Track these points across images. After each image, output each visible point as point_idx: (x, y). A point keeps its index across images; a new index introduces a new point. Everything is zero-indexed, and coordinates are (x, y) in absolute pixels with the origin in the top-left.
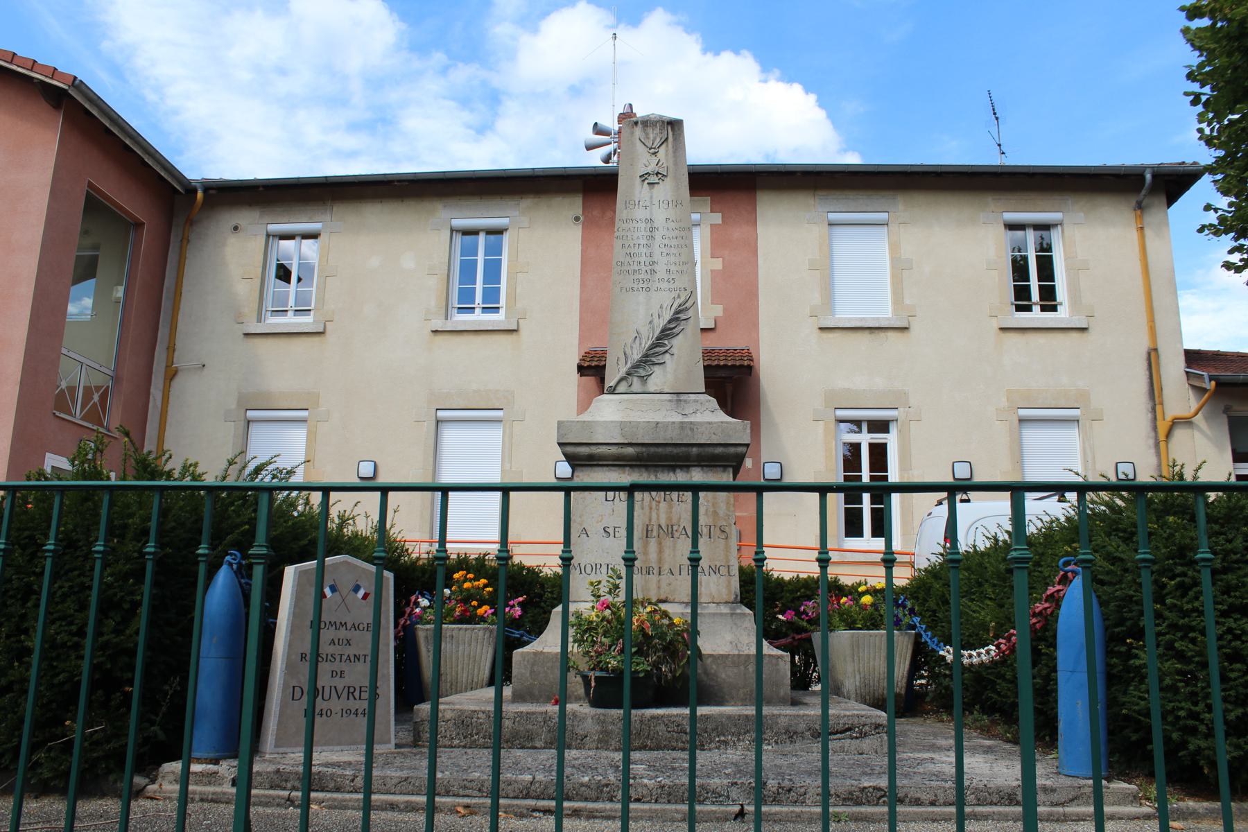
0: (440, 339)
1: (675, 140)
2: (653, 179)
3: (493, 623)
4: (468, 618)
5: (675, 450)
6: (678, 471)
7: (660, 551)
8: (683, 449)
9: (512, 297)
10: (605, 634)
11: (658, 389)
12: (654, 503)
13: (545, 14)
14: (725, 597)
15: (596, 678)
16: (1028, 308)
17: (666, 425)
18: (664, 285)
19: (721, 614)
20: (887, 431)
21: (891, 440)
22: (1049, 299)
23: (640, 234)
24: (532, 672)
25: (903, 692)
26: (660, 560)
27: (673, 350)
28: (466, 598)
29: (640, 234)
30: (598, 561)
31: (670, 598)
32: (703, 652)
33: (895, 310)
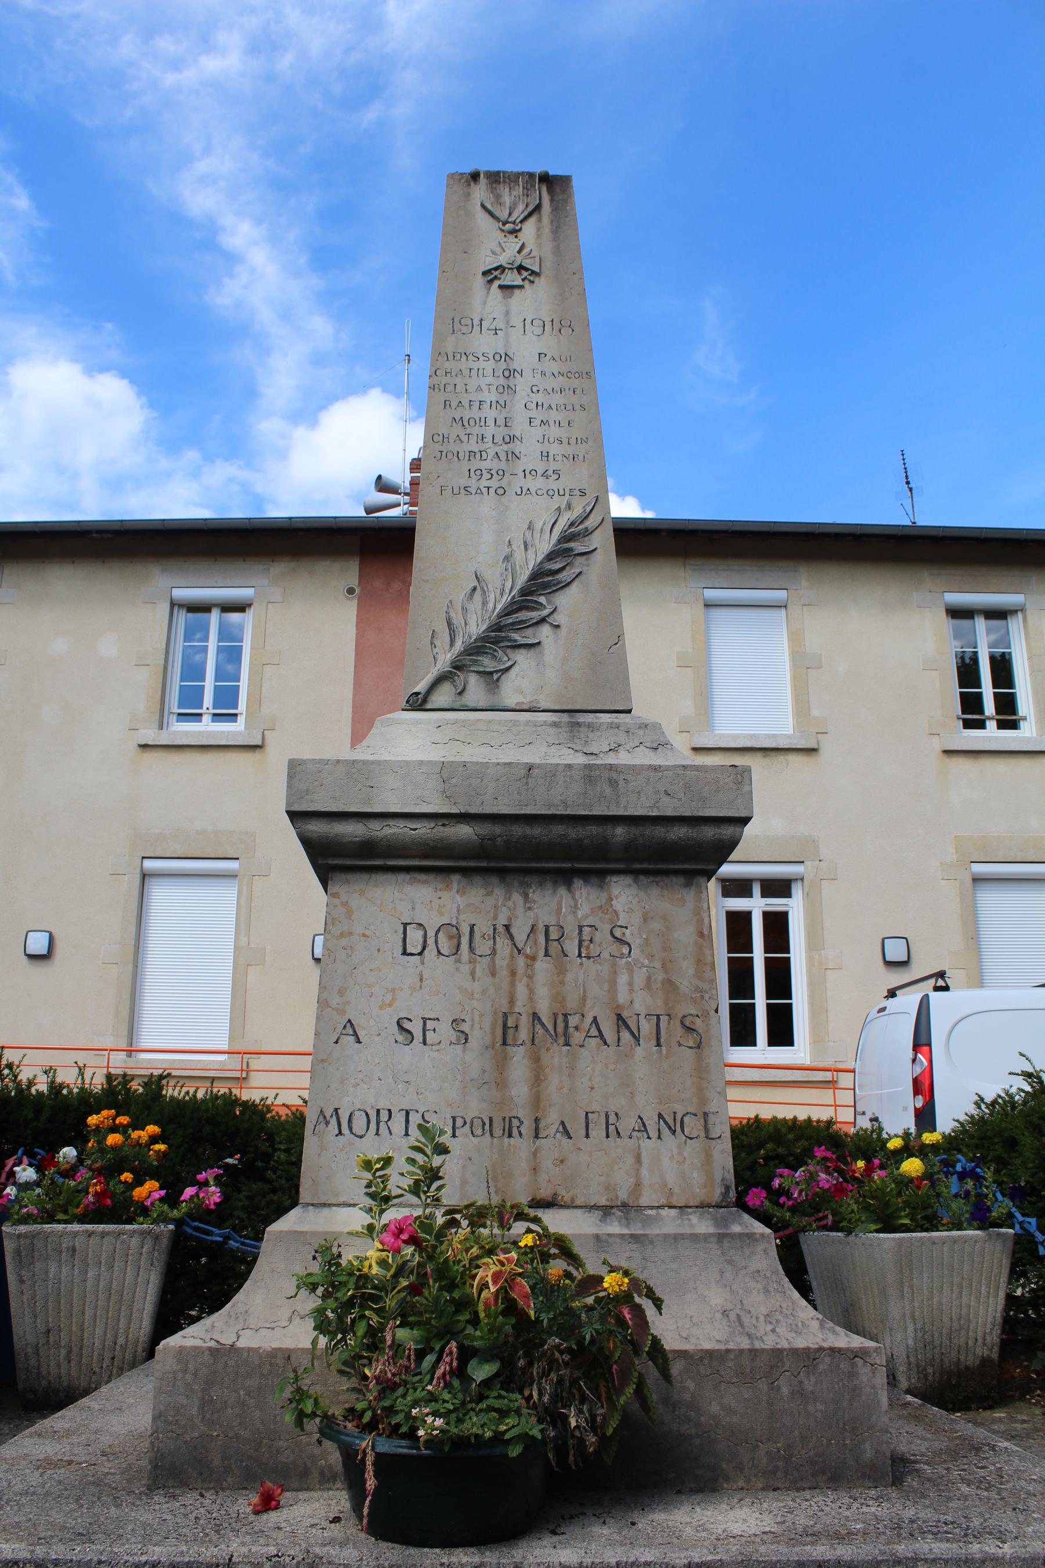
2: (511, 278)
3: (163, 1219)
4: (115, 1210)
6: (578, 883)
7: (538, 1079)
8: (593, 829)
10: (405, 1316)
11: (526, 700)
12: (521, 962)
13: (323, 407)
14: (699, 1193)
15: (379, 1456)
16: (981, 725)
17: (552, 772)
18: (536, 484)
19: (695, 1238)
20: (787, 894)
21: (795, 907)
22: (1008, 714)
23: (483, 382)
24: (206, 1403)
25: (995, 1356)
26: (537, 1101)
27: (559, 618)
28: (113, 1166)
29: (483, 382)
30: (383, 1104)
31: (565, 1195)
32: (666, 1347)
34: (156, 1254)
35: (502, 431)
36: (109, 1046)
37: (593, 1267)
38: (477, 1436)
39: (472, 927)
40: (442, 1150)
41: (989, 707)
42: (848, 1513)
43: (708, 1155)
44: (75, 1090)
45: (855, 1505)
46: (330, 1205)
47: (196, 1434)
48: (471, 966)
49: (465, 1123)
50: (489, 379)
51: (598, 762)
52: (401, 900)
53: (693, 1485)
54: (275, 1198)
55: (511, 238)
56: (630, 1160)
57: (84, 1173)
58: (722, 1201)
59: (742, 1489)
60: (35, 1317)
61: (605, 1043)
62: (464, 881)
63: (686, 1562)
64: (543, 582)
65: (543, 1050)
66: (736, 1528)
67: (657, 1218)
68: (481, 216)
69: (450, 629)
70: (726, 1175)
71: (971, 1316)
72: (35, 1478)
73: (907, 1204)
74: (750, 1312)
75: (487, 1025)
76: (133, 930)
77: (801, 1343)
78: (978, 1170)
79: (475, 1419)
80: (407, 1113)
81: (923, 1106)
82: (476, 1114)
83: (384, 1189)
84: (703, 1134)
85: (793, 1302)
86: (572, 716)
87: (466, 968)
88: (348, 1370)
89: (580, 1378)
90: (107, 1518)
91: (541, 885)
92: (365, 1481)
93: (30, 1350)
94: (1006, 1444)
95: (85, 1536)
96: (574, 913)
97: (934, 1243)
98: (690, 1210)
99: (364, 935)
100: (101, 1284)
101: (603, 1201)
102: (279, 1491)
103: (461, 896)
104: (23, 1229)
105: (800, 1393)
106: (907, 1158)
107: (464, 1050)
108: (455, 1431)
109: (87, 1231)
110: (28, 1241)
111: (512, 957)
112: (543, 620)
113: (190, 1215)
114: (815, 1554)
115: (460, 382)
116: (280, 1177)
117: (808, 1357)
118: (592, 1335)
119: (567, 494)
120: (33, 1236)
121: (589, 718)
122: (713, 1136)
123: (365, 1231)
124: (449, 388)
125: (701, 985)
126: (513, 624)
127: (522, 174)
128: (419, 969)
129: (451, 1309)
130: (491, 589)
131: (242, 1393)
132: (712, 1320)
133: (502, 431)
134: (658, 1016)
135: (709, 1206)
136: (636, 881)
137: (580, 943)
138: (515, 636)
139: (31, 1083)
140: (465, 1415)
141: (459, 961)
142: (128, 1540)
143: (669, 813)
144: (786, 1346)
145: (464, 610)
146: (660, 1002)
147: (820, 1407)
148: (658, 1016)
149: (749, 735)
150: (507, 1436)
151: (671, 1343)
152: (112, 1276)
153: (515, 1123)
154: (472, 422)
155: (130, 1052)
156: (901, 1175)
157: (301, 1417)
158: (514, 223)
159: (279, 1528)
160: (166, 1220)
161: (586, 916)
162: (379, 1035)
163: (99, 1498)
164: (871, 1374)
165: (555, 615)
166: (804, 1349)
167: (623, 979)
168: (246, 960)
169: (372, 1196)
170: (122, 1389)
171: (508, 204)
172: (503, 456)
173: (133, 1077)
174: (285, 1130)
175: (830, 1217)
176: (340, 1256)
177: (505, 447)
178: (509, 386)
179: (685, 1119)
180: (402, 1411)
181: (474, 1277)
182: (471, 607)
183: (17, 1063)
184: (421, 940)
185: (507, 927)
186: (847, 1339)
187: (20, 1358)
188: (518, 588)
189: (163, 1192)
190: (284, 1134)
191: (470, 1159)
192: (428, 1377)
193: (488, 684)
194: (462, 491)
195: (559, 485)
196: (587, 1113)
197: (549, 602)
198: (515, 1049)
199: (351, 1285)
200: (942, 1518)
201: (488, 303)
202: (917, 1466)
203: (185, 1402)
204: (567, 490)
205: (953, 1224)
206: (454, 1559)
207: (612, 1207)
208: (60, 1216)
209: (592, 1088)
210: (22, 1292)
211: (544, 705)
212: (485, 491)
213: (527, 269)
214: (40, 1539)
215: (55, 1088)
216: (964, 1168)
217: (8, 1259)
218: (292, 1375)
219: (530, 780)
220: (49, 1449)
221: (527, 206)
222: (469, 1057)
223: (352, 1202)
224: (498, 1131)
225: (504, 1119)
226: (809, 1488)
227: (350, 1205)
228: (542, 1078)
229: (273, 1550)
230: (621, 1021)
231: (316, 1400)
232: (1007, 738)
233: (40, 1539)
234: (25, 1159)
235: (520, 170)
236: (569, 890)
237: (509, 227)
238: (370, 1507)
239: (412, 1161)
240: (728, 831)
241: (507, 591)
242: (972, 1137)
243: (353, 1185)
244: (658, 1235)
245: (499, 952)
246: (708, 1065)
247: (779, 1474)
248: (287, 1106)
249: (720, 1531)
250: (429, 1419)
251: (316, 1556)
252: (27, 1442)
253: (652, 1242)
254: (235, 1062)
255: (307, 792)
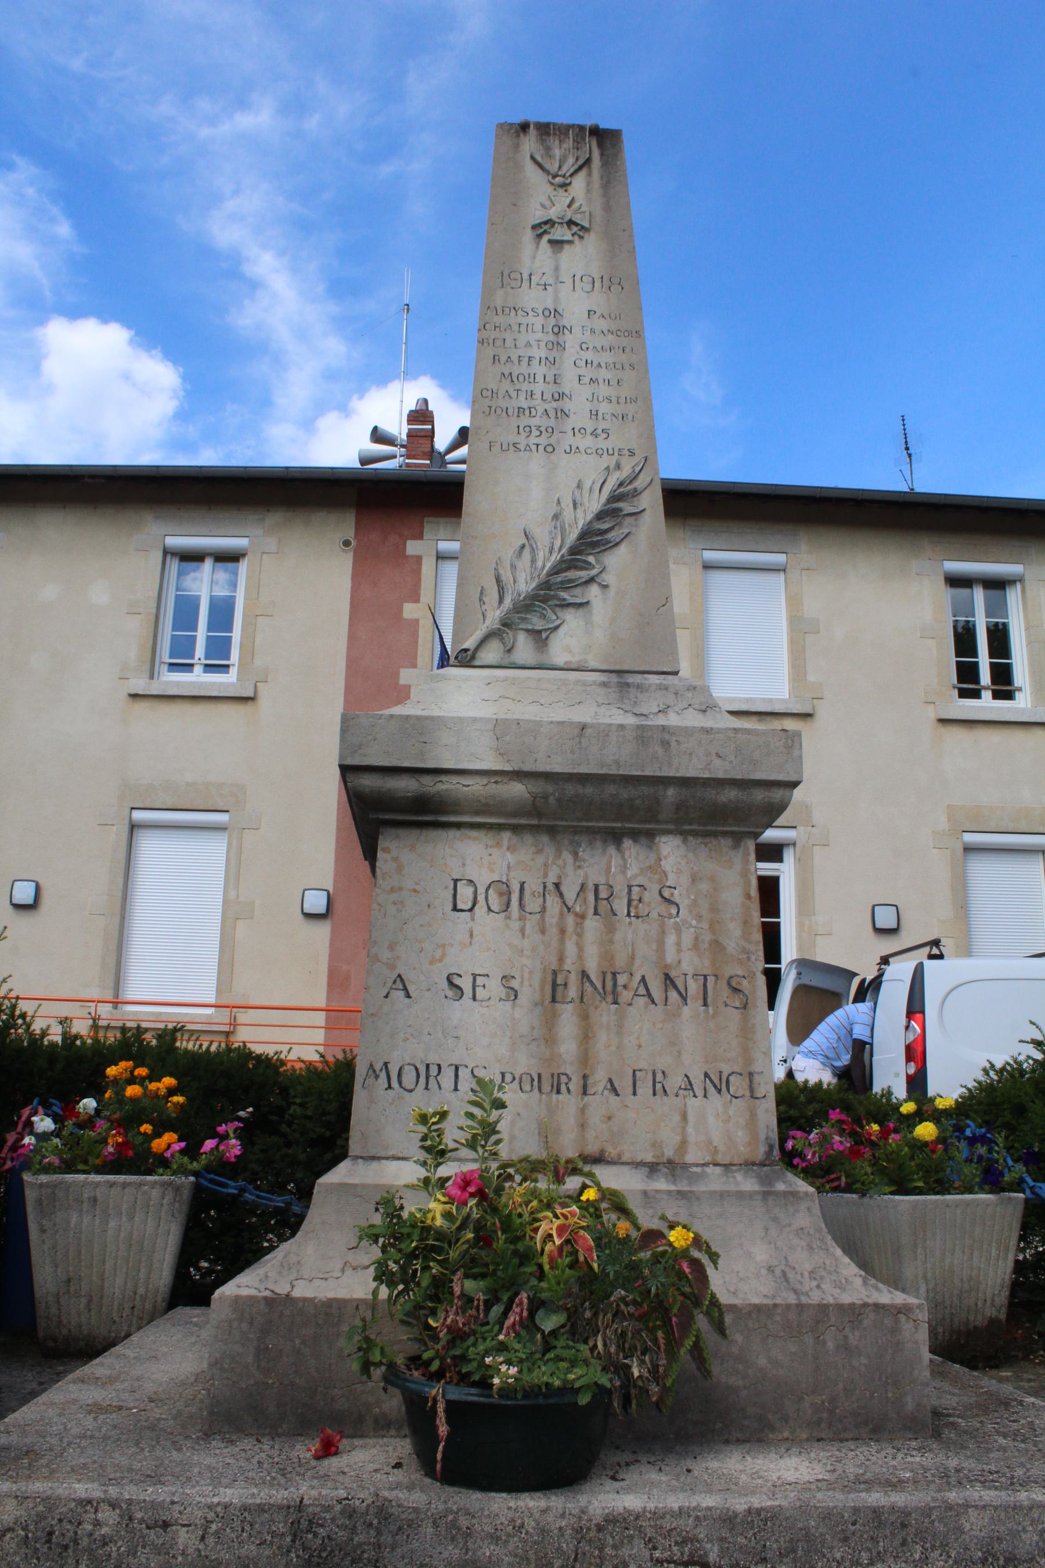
0: (141, 706)
1: (605, 164)
2: (560, 233)
3: (184, 1171)
4: (134, 1161)
5: (625, 793)
6: (627, 843)
7: (586, 1037)
8: (645, 790)
9: (248, 651)
10: (472, 1267)
11: (574, 659)
12: (570, 920)
16: (976, 694)
17: (604, 732)
18: (587, 442)
19: (741, 1195)
20: (780, 860)
21: (786, 872)
22: (1003, 683)
23: (532, 338)
25: (1003, 1316)
26: (585, 1059)
27: (608, 578)
28: (131, 1116)
29: (532, 338)
30: (433, 1058)
31: (611, 1151)
33: (793, 690)
34: (177, 1205)
35: (552, 388)
36: (96, 997)
37: (648, 1221)
38: (547, 1384)
39: (522, 884)
40: (500, 1105)
41: (985, 677)
42: (894, 1463)
43: (753, 1114)
44: (89, 1041)
45: (900, 1456)
46: (379, 1158)
47: (252, 1382)
48: (521, 923)
49: (514, 1079)
50: (539, 335)
51: (650, 723)
52: (451, 856)
53: (739, 1435)
54: (290, 1151)
55: (561, 191)
56: (677, 1118)
57: (102, 1125)
58: (766, 1160)
59: (787, 1439)
60: (56, 1266)
61: (653, 1002)
62: (515, 839)
63: (746, 1507)
64: (593, 541)
65: (592, 1008)
66: (790, 1476)
67: (702, 1176)
68: (530, 168)
69: (499, 586)
70: (771, 1134)
71: (981, 1277)
72: (89, 1422)
73: (920, 1167)
74: (794, 1268)
75: (536, 984)
76: (120, 881)
77: (846, 1299)
78: (988, 1135)
79: (543, 1368)
80: (457, 1068)
81: (915, 1073)
82: (525, 1070)
83: (440, 1143)
84: (748, 1094)
85: (836, 1259)
86: (621, 679)
87: (516, 925)
88: (410, 1320)
89: (641, 1330)
90: (170, 1461)
91: (591, 844)
92: (435, 1428)
93: (50, 1298)
94: (1032, 1399)
95: (154, 1478)
96: (624, 873)
97: (948, 1206)
98: (734, 1168)
99: (415, 891)
100: (122, 1235)
101: (649, 1158)
102: (338, 1437)
103: (512, 853)
104: (44, 1178)
105: (845, 1348)
106: (920, 1123)
107: (514, 1007)
108: (528, 1379)
109: (108, 1182)
110: (49, 1190)
111: (562, 915)
112: (592, 580)
113: (208, 1169)
114: (870, 1500)
115: (508, 336)
116: (294, 1131)
117: (853, 1313)
118: (657, 1288)
119: (616, 454)
120: (55, 1186)
121: (637, 679)
122: (758, 1096)
123: (421, 1185)
124: (499, 343)
125: (747, 946)
126: (562, 582)
127: (573, 126)
128: (469, 925)
129: (516, 1261)
130: (540, 547)
131: (297, 1342)
132: (758, 1276)
133: (552, 388)
134: (705, 977)
135: (753, 1164)
136: (685, 841)
137: (629, 905)
138: (564, 595)
139: (44, 1033)
140: (533, 1364)
141: (509, 918)
142: (197, 1482)
143: (720, 775)
144: (832, 1301)
145: (513, 567)
146: (707, 963)
147: (864, 1360)
148: (705, 977)
149: (745, 698)
150: (577, 1385)
151: (724, 1299)
152: (132, 1227)
153: (564, 1079)
154: (521, 379)
155: (116, 1004)
156: (914, 1139)
157: (366, 1366)
158: (564, 176)
159: (344, 1473)
160: (186, 1173)
161: (636, 876)
162: (429, 990)
163: (158, 1442)
164: (913, 1330)
165: (603, 575)
166: (850, 1305)
167: (671, 939)
168: (234, 912)
169: (428, 1150)
170: (152, 1338)
171: (558, 158)
172: (552, 414)
173: (147, 1030)
174: (300, 1084)
175: (843, 1179)
176: (402, 1208)
177: (555, 404)
178: (558, 343)
179: (731, 1079)
180: (474, 1359)
181: (536, 1230)
182: (520, 565)
183: (30, 1013)
184: (471, 897)
185: (557, 885)
186: (890, 1295)
187: (41, 1310)
188: (567, 546)
189: (183, 1144)
190: (299, 1088)
191: (519, 1114)
192: (497, 1328)
193: (536, 642)
194: (511, 448)
195: (608, 444)
196: (634, 1071)
197: (597, 561)
198: (564, 1006)
199: (416, 1237)
200: (986, 1468)
201: (537, 258)
202: (951, 1419)
203: (241, 1350)
204: (616, 450)
205: (965, 1187)
206: (521, 1503)
207: (658, 1164)
208: (80, 1167)
209: (640, 1046)
210: (43, 1242)
211: (593, 664)
212: (534, 448)
213: (576, 224)
214: (110, 1480)
215: (69, 1039)
216: (974, 1134)
217: (30, 1209)
218: (360, 1324)
219: (583, 740)
220: (95, 1395)
221: (577, 160)
222: (518, 1013)
223: (401, 1155)
224: (546, 1087)
225: (553, 1075)
226: (852, 1439)
227: (399, 1159)
228: (590, 1035)
229: (342, 1493)
230: (669, 981)
231: (382, 1349)
232: (1001, 709)
233: (110, 1480)
234: (40, 1109)
235: (570, 122)
236: (618, 848)
237: (558, 180)
238: (444, 1453)
239: (470, 1115)
240: (777, 794)
241: (556, 549)
242: (980, 1103)
243: (407, 1139)
244: (704, 1192)
245: (548, 909)
246: (754, 1025)
247: (823, 1425)
248: (302, 1061)
249: (775, 1478)
250: (504, 1368)
251: (386, 1499)
252: (72, 1387)
253: (698, 1199)
254: (224, 1016)
255: (360, 746)
